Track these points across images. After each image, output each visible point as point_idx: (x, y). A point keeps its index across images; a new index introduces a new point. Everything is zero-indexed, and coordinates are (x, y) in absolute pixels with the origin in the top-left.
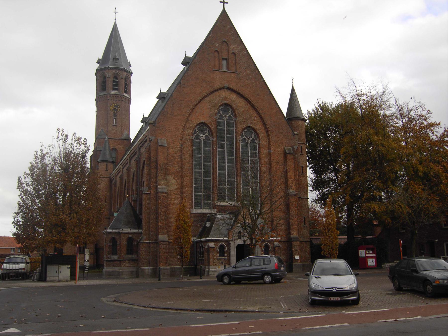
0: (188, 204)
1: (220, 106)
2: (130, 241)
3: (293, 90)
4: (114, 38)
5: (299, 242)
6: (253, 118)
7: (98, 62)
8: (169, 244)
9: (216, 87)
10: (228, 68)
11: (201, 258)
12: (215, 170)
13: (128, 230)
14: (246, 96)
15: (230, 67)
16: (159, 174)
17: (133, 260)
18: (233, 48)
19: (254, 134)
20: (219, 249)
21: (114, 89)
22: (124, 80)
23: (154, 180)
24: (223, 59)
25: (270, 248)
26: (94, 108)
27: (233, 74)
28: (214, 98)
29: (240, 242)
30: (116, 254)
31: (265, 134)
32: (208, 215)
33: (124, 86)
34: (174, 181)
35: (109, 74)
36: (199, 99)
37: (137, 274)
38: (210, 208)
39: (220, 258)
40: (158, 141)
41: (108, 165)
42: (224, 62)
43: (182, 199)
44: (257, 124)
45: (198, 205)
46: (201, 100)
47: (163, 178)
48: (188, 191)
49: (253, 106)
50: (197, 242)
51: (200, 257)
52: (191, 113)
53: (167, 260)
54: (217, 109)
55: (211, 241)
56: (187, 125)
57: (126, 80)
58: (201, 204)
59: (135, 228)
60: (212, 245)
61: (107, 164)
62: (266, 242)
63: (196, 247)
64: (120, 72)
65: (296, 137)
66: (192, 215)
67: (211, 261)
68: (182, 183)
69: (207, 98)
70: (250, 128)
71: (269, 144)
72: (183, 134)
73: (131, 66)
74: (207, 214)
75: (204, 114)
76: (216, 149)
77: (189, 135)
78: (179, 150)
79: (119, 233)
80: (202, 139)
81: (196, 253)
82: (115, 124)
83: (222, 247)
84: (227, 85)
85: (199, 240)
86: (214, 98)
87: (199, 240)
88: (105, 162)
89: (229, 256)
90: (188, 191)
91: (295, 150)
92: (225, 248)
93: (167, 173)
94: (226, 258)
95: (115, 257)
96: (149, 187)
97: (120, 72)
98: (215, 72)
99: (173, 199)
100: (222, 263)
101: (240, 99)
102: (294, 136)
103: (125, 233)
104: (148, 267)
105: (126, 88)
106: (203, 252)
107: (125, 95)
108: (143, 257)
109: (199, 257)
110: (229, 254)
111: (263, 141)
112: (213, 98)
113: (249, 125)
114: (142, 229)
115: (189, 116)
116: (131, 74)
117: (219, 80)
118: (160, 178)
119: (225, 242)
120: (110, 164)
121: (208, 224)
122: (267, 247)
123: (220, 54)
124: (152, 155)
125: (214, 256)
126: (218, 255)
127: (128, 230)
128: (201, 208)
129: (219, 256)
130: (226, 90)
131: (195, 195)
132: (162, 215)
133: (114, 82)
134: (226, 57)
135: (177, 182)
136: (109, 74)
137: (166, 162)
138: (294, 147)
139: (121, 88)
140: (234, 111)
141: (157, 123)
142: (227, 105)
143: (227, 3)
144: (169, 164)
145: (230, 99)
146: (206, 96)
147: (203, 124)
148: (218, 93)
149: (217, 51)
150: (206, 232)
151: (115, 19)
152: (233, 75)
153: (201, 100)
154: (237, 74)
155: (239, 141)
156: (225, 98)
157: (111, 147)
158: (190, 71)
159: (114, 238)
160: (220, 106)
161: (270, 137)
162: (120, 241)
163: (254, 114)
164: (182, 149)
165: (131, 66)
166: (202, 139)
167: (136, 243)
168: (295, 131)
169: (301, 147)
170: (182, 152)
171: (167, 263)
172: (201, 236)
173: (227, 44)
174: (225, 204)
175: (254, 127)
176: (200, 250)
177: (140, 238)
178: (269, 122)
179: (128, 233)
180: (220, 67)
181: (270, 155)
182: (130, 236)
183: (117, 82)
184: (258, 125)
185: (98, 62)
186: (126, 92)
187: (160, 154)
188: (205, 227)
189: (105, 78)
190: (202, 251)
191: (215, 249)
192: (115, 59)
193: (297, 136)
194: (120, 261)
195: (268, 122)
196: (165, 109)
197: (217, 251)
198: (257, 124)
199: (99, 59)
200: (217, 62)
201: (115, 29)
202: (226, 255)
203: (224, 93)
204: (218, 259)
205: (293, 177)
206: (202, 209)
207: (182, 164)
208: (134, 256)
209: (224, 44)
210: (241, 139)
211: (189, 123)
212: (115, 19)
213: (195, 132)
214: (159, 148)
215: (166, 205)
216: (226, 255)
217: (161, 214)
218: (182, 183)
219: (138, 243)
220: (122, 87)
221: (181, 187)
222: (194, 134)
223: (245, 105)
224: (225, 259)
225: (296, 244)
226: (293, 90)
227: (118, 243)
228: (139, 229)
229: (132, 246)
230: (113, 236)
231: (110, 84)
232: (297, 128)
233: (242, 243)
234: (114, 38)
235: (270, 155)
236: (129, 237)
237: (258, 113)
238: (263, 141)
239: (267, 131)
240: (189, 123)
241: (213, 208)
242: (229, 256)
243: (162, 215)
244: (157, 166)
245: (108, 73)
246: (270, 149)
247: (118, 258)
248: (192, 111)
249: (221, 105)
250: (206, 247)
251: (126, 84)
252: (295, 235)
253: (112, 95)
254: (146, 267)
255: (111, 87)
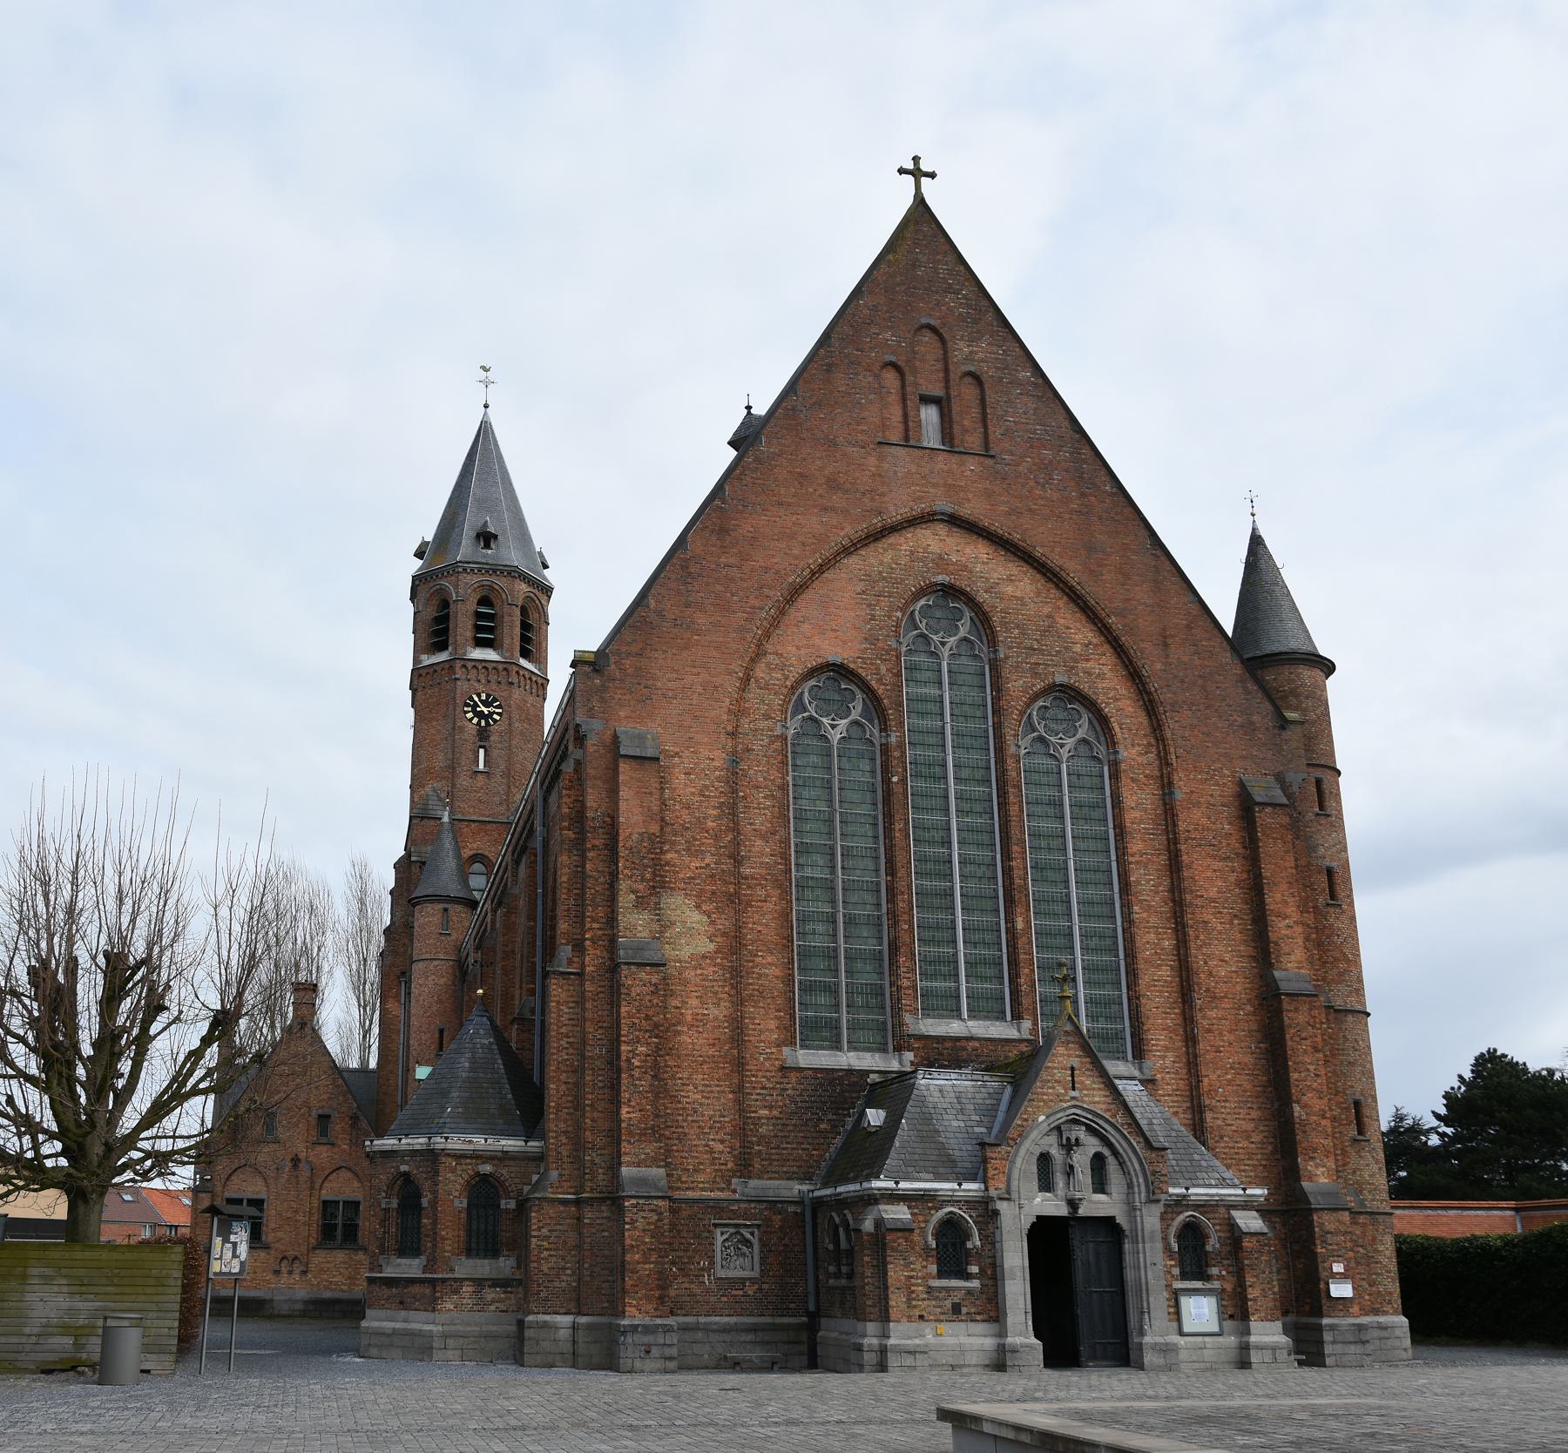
0: (764, 1024)
1: (917, 596)
2: (484, 1191)
3: (1256, 542)
4: (483, 456)
5: (1345, 1216)
6: (1077, 648)
7: (419, 554)
8: (673, 1211)
9: (895, 513)
10: (947, 434)
11: (843, 1282)
12: (901, 873)
13: (479, 1142)
14: (1039, 552)
15: (957, 430)
16: (623, 885)
17: (496, 1283)
18: (968, 351)
19: (1085, 717)
20: (938, 1235)
21: (480, 643)
22: (518, 612)
23: (601, 912)
24: (926, 400)
25: (1212, 1244)
26: (410, 714)
27: (970, 459)
28: (888, 558)
29: (1050, 1205)
30: (416, 1253)
31: (1142, 718)
32: (874, 1078)
33: (518, 631)
34: (695, 918)
35: (465, 596)
36: (814, 561)
37: (516, 1350)
38: (883, 1049)
39: (944, 1283)
40: (615, 737)
41: (451, 912)
42: (930, 414)
43: (739, 1001)
44: (1101, 676)
45: (823, 1033)
46: (821, 569)
47: (640, 903)
48: (768, 967)
49: (1075, 597)
50: (818, 1204)
51: (838, 1275)
52: (775, 622)
53: (663, 1288)
54: (903, 610)
55: (893, 1197)
56: (760, 671)
57: (524, 611)
58: (835, 1026)
59: (513, 1135)
60: (899, 1213)
61: (446, 910)
62: (1188, 1207)
63: (815, 1226)
64: (501, 582)
65: (1293, 734)
66: (793, 1077)
67: (897, 1300)
68: (738, 928)
69: (852, 562)
70: (1069, 694)
71: (1164, 760)
72: (738, 712)
73: (546, 566)
74: (865, 1073)
75: (834, 626)
76: (903, 781)
77: (767, 717)
78: (718, 779)
79: (431, 1156)
80: (836, 736)
81: (816, 1259)
82: (481, 766)
83: (951, 1231)
84: (949, 509)
85: (828, 1192)
86: (888, 558)
87: (828, 1192)
88: (439, 901)
89: (993, 1276)
90: (768, 967)
91: (1295, 788)
92: (968, 1236)
93: (658, 884)
94: (975, 1284)
95: (410, 1267)
96: (579, 947)
97: (501, 582)
98: (886, 449)
99: (694, 1002)
100: (956, 1309)
101: (1014, 568)
102: (1283, 728)
103: (460, 1156)
104: (569, 1319)
105: (525, 639)
106: (850, 1253)
107: (523, 662)
108: (545, 1268)
109: (829, 1276)
110: (994, 1265)
111: (1134, 752)
112: (879, 558)
113: (1060, 679)
114: (542, 1137)
115: (767, 635)
116: (547, 591)
117: (906, 483)
118: (625, 900)
119: (969, 1203)
120: (458, 908)
121: (875, 1117)
122: (1191, 1235)
123: (910, 378)
124: (591, 801)
125: (910, 1271)
126: (933, 1268)
127: (479, 1142)
128: (836, 1046)
129: (941, 1274)
130: (941, 529)
131: (807, 988)
132: (636, 1073)
133: (479, 616)
134: (937, 391)
135: (713, 923)
136: (465, 596)
137: (654, 828)
138: (1290, 777)
139: (507, 641)
140: (982, 619)
141: (612, 659)
142: (949, 591)
143: (932, 175)
144: (673, 843)
145: (965, 568)
146: (847, 551)
147: (840, 671)
148: (905, 542)
149: (893, 365)
150: (868, 1152)
151: (486, 406)
152: (972, 465)
153: (821, 569)
154: (989, 462)
155: (1013, 749)
156: (941, 562)
157: (466, 853)
158: (769, 444)
159: (406, 1175)
160: (917, 596)
161: (1168, 733)
162: (435, 1193)
163: (1082, 634)
164: (734, 775)
165: (546, 566)
166: (836, 736)
167: (512, 1205)
168: (1290, 707)
169: (1319, 782)
170: (734, 791)
171: (661, 1299)
172: (832, 1179)
173: (943, 340)
174: (954, 1028)
175: (1085, 687)
176: (837, 1243)
177: (535, 1178)
178: (1159, 666)
179: (477, 1156)
180: (909, 428)
181: (1168, 812)
182: (487, 1168)
183: (490, 617)
184: (1103, 678)
185: (419, 554)
186: (525, 653)
187: (624, 793)
188: (860, 1130)
189: (445, 604)
190: (844, 1245)
191: (916, 1237)
192: (486, 538)
193: (1298, 729)
194: (433, 1282)
195: (1152, 665)
196: (652, 603)
197: (926, 1248)
198: (1101, 676)
199: (424, 544)
200: (896, 413)
201: (486, 432)
202: (974, 1269)
203: (935, 541)
204: (930, 1290)
205: (1291, 910)
206: (840, 1049)
207: (736, 843)
208: (504, 1265)
209: (927, 337)
210: (1025, 743)
211: (768, 665)
212: (486, 406)
213: (800, 707)
214: (624, 767)
215: (656, 1026)
216: (974, 1269)
217: (631, 1068)
218: (738, 928)
219: (523, 1206)
220: (512, 632)
221: (734, 946)
222: (794, 715)
223: (1038, 594)
224: (969, 1292)
225: (1329, 1227)
226: (1256, 542)
227: (425, 1202)
228: (529, 1137)
229: (494, 1216)
230: (404, 1168)
231: (463, 626)
232: (1293, 700)
233: (1063, 1211)
234: (483, 456)
235: (1168, 812)
236: (478, 1174)
237: (1105, 631)
238: (1134, 752)
239: (1149, 705)
240: (768, 665)
241: (898, 1049)
242: (994, 1277)
243: (636, 1073)
244: (612, 849)
245: (456, 586)
246: (1170, 784)
247: (425, 1269)
248: (782, 612)
249: (921, 593)
250: (868, 1225)
251: (526, 626)
252: (1323, 1180)
253: (470, 665)
254: (559, 1318)
255: (469, 634)
